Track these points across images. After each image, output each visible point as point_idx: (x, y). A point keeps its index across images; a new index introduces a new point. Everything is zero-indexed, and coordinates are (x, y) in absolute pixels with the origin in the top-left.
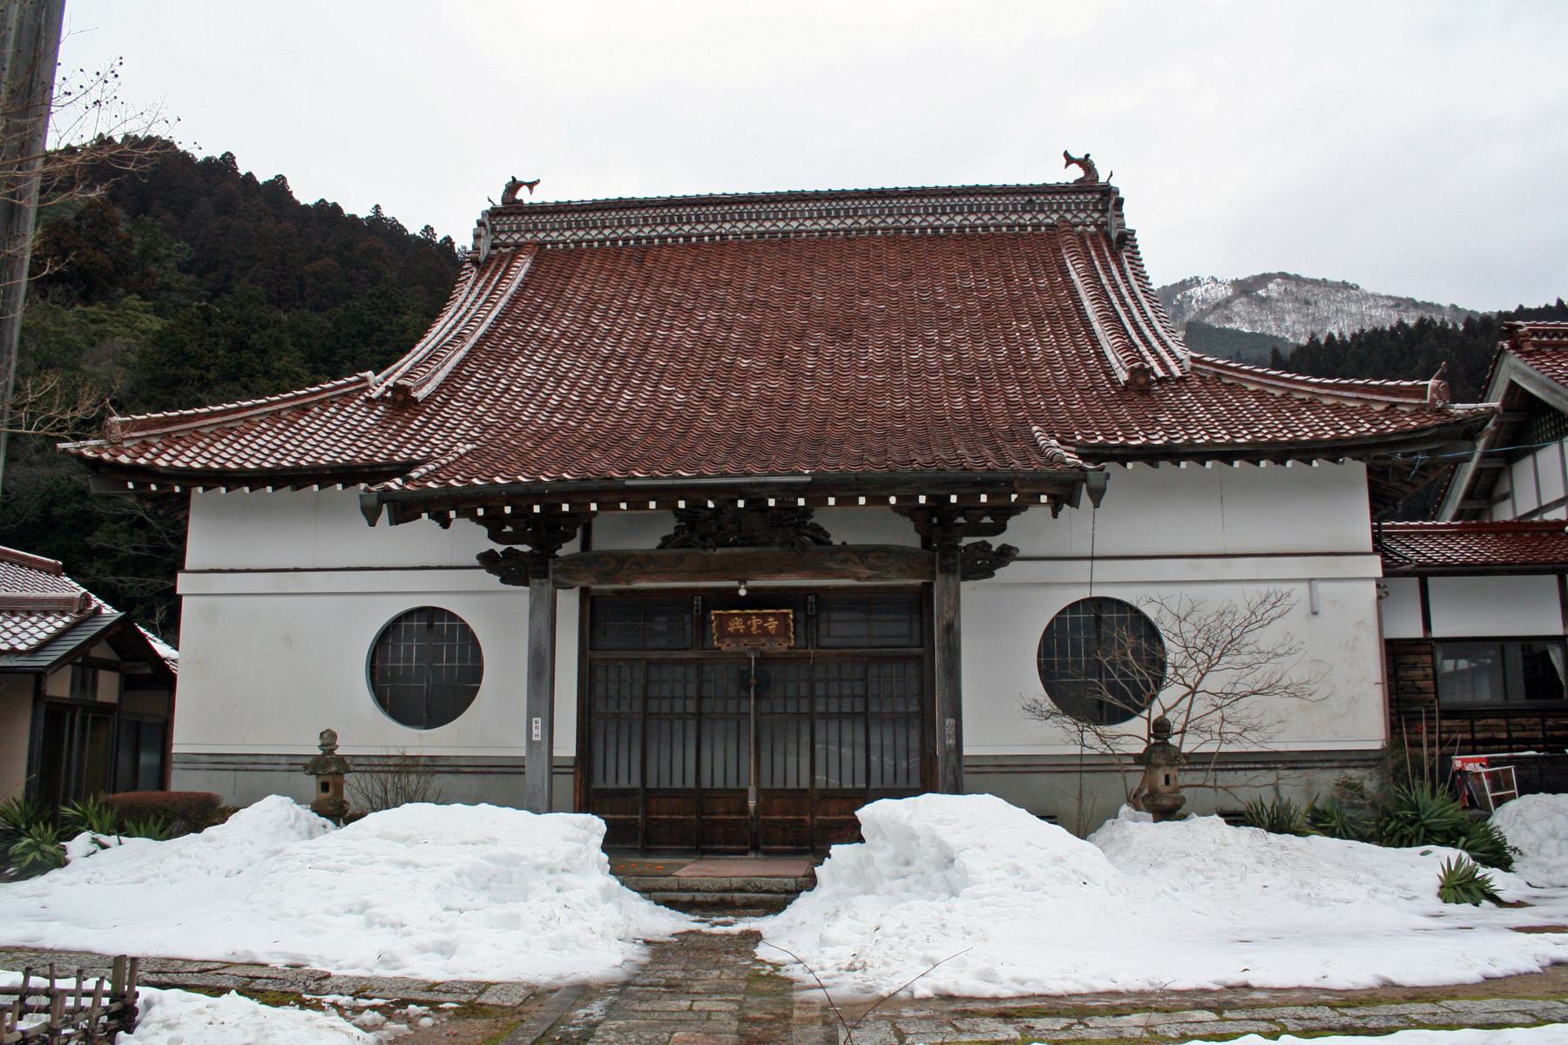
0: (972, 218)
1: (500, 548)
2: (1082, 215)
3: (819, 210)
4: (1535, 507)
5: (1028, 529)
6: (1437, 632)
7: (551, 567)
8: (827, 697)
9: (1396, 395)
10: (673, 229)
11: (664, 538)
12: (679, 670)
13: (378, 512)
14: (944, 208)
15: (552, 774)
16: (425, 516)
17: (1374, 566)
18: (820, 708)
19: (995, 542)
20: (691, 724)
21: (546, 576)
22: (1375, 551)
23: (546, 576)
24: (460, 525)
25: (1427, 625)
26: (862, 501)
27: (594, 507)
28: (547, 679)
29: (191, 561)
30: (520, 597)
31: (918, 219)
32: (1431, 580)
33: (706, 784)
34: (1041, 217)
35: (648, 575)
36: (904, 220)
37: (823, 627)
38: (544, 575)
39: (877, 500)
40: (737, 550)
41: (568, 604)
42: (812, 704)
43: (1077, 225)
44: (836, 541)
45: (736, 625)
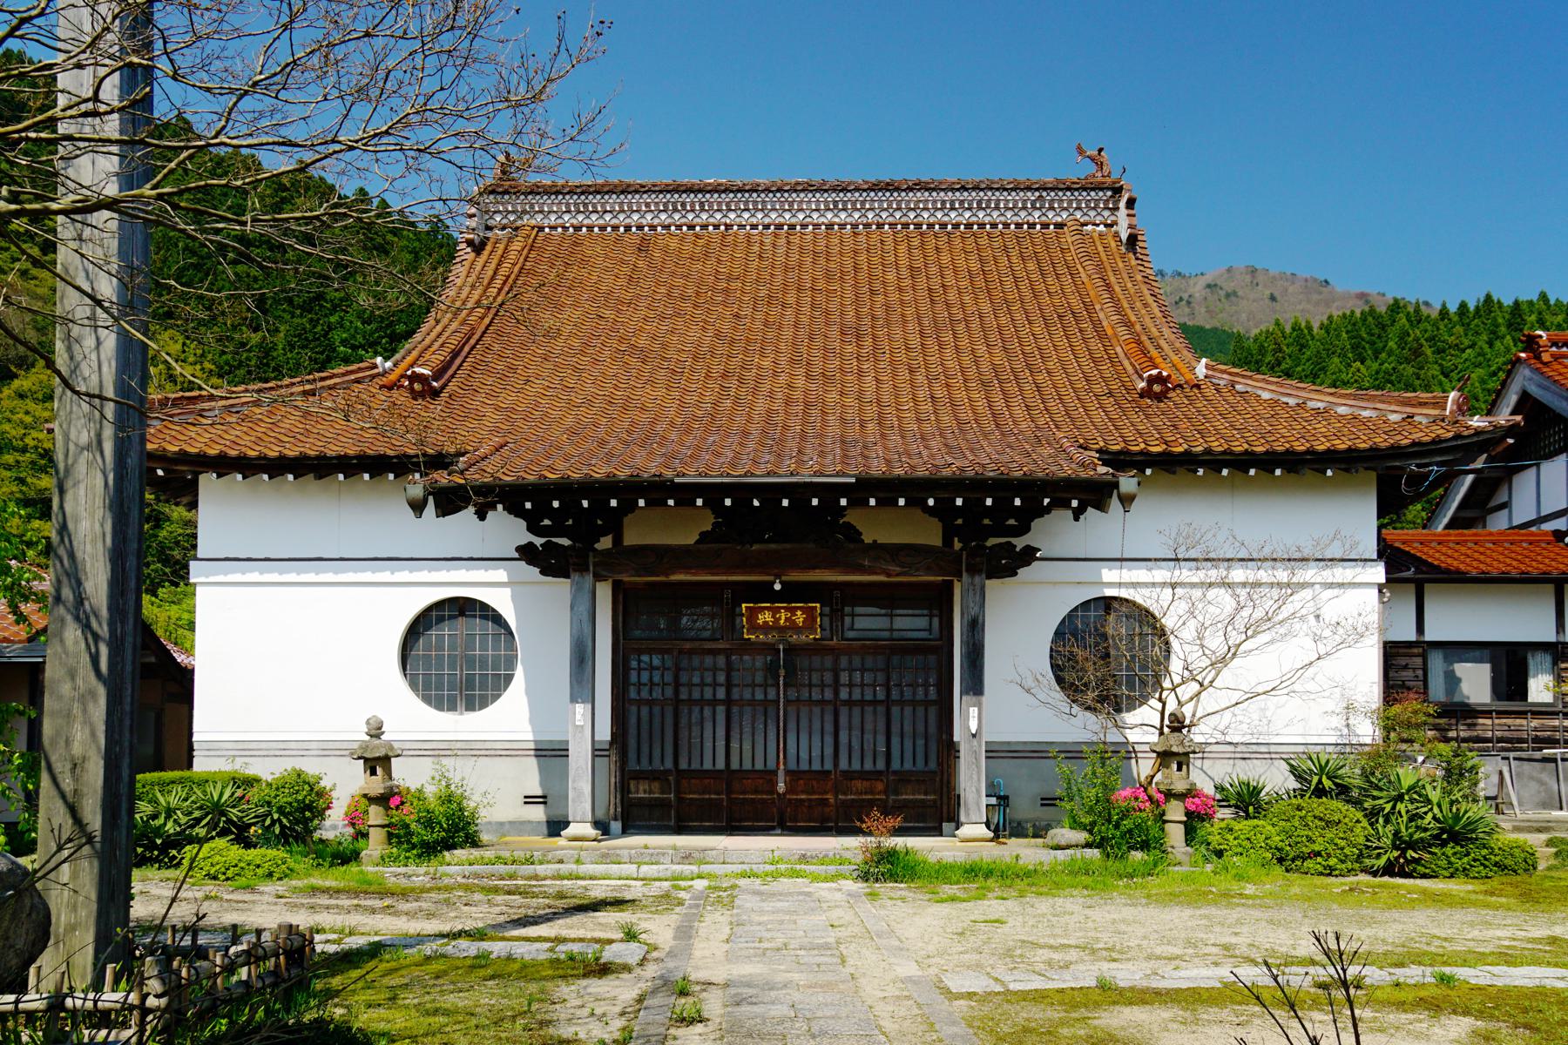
0: (981, 214)
1: (539, 541)
2: (1092, 213)
3: (826, 202)
4: (1534, 517)
5: (1055, 532)
6: (1430, 636)
7: (591, 560)
8: (851, 685)
9: (1413, 406)
10: (677, 216)
11: (702, 534)
12: (708, 660)
13: (425, 502)
14: (952, 202)
15: (594, 756)
16: (500, 507)
17: (1378, 573)
18: (844, 694)
19: (1020, 543)
20: (721, 710)
21: (587, 570)
22: (1380, 555)
23: (587, 570)
24: (499, 516)
25: (1420, 628)
26: (902, 502)
27: (843, 502)
28: (589, 669)
29: (206, 544)
30: (561, 589)
31: (926, 215)
32: (1427, 586)
33: (735, 765)
34: (1051, 214)
35: (686, 568)
36: (912, 215)
37: (848, 620)
38: (582, 569)
39: (916, 502)
40: (773, 546)
41: (604, 592)
42: (836, 693)
43: (1086, 224)
44: (868, 539)
45: (765, 617)
